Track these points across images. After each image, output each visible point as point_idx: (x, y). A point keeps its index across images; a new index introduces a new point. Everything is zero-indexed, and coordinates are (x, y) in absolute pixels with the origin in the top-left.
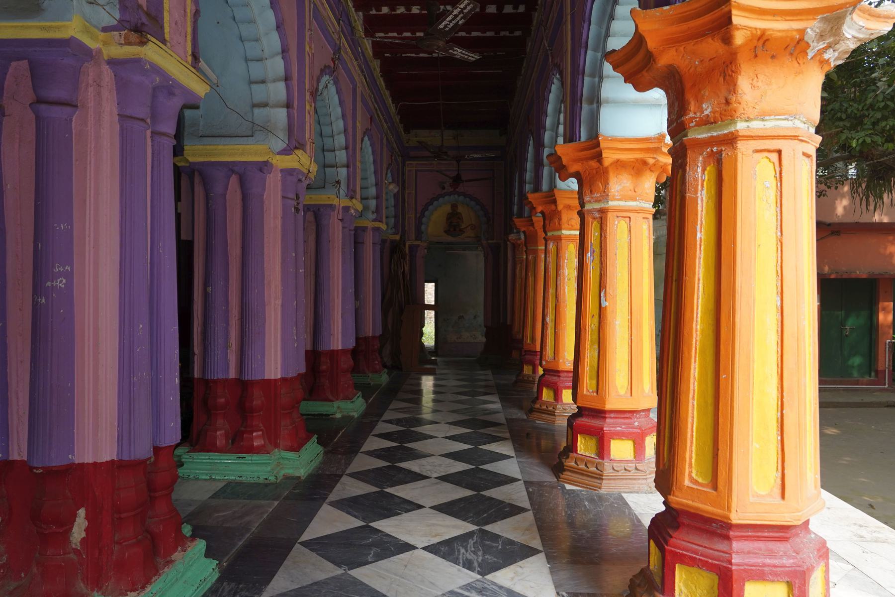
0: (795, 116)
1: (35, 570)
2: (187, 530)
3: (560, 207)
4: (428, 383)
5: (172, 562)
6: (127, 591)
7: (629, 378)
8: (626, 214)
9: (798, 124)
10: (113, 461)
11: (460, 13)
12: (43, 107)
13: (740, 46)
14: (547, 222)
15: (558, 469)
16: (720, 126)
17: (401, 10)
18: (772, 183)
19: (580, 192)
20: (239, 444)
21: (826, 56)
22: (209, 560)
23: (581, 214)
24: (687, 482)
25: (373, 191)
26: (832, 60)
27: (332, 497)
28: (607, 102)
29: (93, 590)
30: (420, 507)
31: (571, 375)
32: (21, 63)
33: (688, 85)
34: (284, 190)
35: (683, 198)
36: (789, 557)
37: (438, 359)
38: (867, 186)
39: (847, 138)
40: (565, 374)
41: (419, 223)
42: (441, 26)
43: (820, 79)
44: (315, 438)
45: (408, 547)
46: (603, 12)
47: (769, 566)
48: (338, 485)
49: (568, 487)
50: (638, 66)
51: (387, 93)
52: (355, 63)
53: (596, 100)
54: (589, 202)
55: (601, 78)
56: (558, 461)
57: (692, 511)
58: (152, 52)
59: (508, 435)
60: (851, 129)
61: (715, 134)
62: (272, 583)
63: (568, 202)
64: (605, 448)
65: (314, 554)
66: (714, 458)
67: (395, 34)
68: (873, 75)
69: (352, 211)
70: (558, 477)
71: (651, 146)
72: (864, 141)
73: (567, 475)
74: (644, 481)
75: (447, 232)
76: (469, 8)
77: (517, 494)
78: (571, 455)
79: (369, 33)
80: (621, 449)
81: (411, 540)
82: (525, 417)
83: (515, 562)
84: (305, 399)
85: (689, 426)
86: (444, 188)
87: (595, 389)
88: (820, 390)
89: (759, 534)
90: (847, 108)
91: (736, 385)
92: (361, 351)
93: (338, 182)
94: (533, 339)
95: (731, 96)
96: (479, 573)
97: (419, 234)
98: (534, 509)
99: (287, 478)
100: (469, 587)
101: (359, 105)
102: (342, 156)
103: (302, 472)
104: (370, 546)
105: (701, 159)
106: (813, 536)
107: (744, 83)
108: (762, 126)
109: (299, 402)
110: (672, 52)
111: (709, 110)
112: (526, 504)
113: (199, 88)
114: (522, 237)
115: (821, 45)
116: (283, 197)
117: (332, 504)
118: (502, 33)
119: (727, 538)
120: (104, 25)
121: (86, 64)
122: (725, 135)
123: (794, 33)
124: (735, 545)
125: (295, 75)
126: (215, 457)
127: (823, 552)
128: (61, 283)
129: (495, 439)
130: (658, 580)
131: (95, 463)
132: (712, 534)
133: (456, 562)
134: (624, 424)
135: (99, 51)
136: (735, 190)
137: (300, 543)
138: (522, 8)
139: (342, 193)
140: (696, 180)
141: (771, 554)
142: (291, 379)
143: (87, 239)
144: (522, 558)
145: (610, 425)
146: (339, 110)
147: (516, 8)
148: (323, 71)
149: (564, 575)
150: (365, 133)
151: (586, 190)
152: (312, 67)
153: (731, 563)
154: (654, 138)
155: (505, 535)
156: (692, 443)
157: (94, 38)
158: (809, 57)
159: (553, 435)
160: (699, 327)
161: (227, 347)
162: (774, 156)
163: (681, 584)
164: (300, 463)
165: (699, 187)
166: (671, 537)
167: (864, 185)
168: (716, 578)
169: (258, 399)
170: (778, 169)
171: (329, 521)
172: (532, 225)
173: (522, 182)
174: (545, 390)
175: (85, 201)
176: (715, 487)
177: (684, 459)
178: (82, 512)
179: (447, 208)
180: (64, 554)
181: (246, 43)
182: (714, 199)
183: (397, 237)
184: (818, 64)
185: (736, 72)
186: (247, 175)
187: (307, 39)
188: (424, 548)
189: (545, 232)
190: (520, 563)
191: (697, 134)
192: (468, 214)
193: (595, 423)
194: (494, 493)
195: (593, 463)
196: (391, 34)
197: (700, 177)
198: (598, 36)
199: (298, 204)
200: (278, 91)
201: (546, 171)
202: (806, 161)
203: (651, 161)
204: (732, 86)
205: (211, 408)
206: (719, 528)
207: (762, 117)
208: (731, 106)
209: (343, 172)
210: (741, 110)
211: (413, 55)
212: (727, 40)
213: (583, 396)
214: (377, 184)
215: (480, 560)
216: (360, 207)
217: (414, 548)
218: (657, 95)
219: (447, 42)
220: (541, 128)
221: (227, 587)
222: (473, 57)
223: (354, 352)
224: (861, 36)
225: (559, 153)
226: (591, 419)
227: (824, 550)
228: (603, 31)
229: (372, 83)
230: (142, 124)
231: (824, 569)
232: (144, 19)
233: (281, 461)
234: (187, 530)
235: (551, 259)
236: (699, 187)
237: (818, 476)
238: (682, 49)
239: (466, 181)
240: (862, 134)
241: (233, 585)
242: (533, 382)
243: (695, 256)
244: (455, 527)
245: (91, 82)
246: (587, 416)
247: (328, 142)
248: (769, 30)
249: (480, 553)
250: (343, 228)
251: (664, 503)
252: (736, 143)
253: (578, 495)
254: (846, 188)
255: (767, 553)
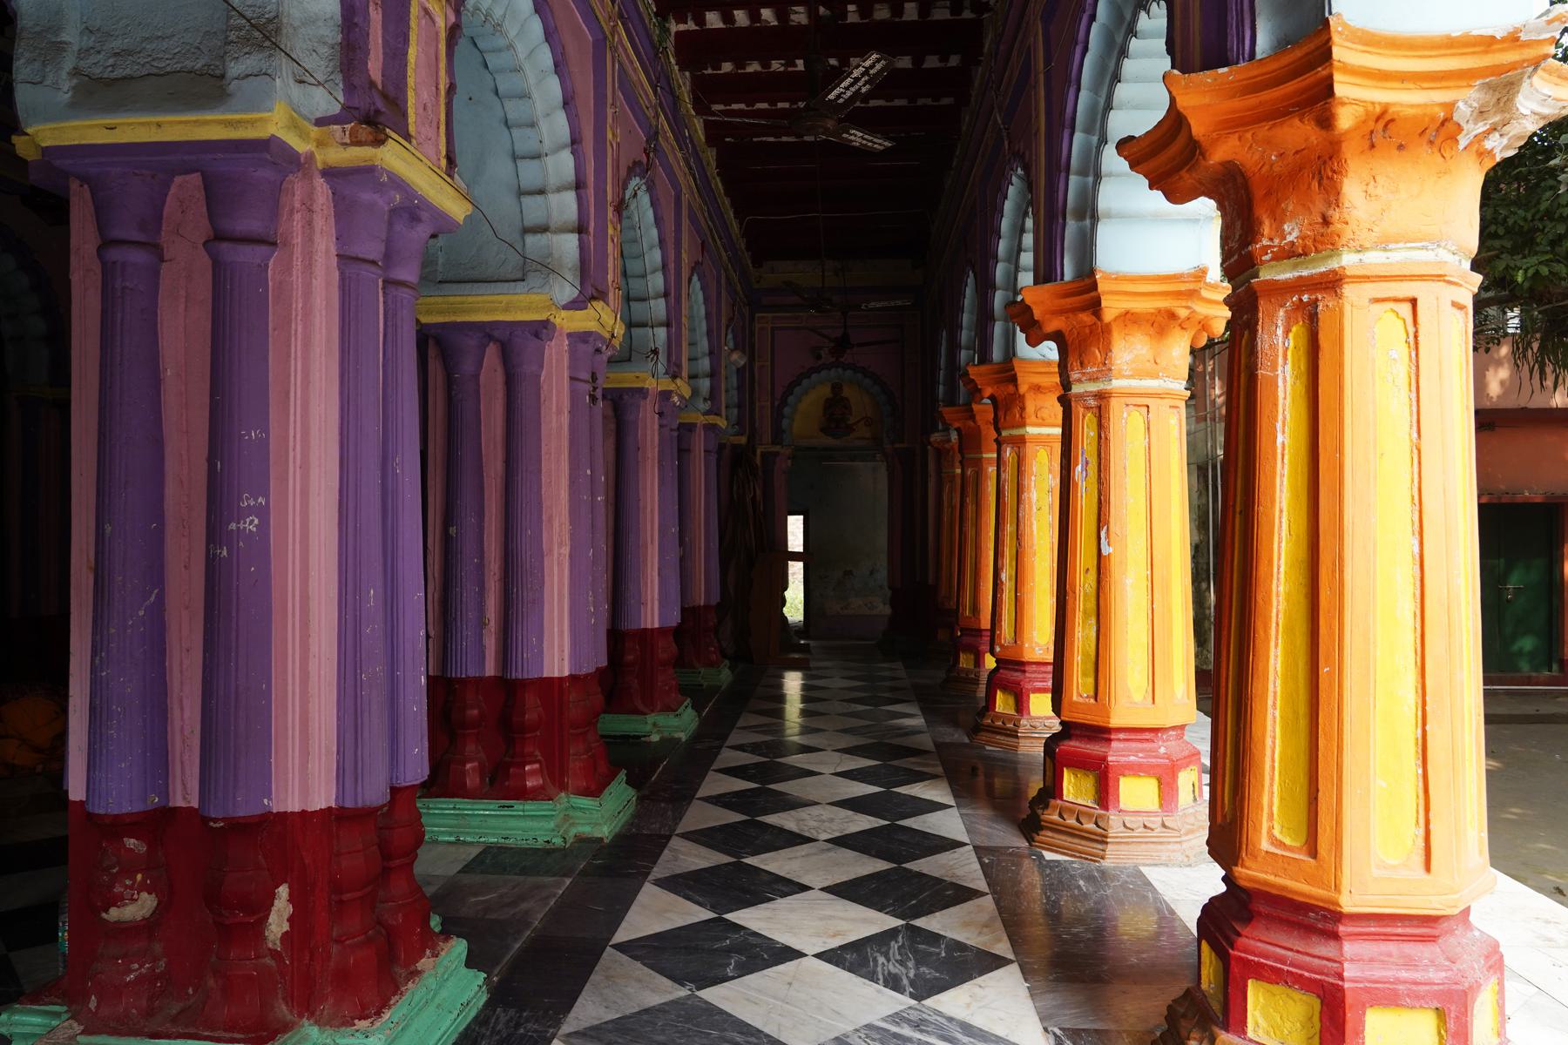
0: (1437, 243)
1: (211, 982)
2: (435, 922)
3: (1023, 389)
4: (793, 683)
5: (418, 973)
6: (353, 1019)
7: (1150, 669)
8: (1143, 401)
9: (1444, 255)
10: (330, 808)
11: (863, 75)
12: (225, 246)
13: (1347, 132)
14: (1001, 414)
15: (1030, 827)
16: (1313, 260)
17: (754, 67)
18: (1402, 352)
19: (1063, 366)
20: (502, 784)
21: (1488, 144)
22: (472, 972)
23: (1065, 401)
24: (1265, 845)
25: (705, 364)
26: (1497, 151)
27: (658, 872)
28: (1109, 216)
29: (301, 1016)
30: (805, 888)
31: (1050, 668)
32: (188, 177)
33: (1258, 193)
34: (572, 367)
35: (1252, 378)
36: (1439, 968)
37: (812, 643)
38: (1542, 348)
39: (1507, 267)
40: (1034, 668)
41: (778, 416)
42: (831, 96)
43: (1479, 180)
44: (622, 775)
45: (790, 954)
46: (1101, 69)
47: (1405, 982)
48: (666, 851)
49: (1049, 856)
50: (1169, 160)
51: (727, 201)
52: (679, 155)
53: (1089, 211)
54: (1079, 381)
55: (1098, 177)
56: (1030, 815)
57: (1274, 891)
58: (392, 156)
59: (939, 770)
60: (1513, 251)
61: (1305, 273)
62: (575, 1009)
63: (1036, 380)
64: (1111, 790)
65: (639, 964)
66: (1310, 804)
67: (742, 106)
68: (1552, 163)
69: (676, 399)
70: (1030, 840)
71: (1183, 287)
72: (1537, 272)
73: (1046, 836)
74: (1177, 847)
75: (824, 430)
76: (878, 67)
77: (964, 867)
78: (1052, 802)
79: (701, 107)
80: (1136, 793)
81: (795, 944)
82: (967, 740)
83: (971, 978)
84: (605, 712)
85: (1268, 752)
86: (819, 357)
87: (1092, 693)
88: (1487, 694)
89: (1389, 930)
90: (1506, 217)
91: (1347, 684)
92: (691, 628)
93: (655, 352)
94: (976, 609)
95: (1331, 212)
96: (912, 996)
97: (778, 435)
98: (994, 892)
99: (581, 840)
100: (897, 1018)
101: (685, 222)
102: (659, 308)
103: (605, 831)
104: (728, 951)
105: (1281, 313)
106: (1477, 933)
107: (1352, 189)
108: (1384, 260)
109: (597, 715)
110: (1233, 141)
111: (1295, 234)
112: (981, 885)
113: (457, 209)
114: (954, 436)
115: (1481, 128)
116: (572, 378)
117: (660, 883)
118: (921, 102)
119: (1336, 937)
120: (319, 115)
121: (291, 177)
122: (1322, 274)
123: (1437, 109)
124: (1349, 948)
125: (591, 179)
126: (466, 806)
127: (1495, 961)
128: (251, 524)
129: (919, 777)
130: (1216, 1006)
131: (304, 812)
132: (1309, 930)
133: (872, 977)
134: (1142, 751)
135: (310, 157)
136: (1341, 365)
137: (613, 946)
138: (954, 61)
139: (661, 368)
140: (1273, 347)
141: (1410, 963)
142: (586, 676)
143: (291, 454)
144: (982, 973)
145: (1117, 753)
146: (654, 232)
147: (944, 59)
148: (631, 172)
149: (1050, 1000)
150: (693, 270)
151: (1073, 362)
152: (617, 167)
153: (1341, 977)
154: (1189, 275)
155: (949, 935)
156: (1272, 779)
157: (304, 136)
158: (1461, 147)
159: (1015, 769)
160: (1281, 588)
161: (482, 624)
162: (1406, 309)
163: (1257, 1013)
164: (599, 816)
165: (1280, 360)
166: (1239, 935)
167: (1536, 346)
168: (1317, 1003)
169: (532, 710)
170: (1411, 330)
171: (655, 912)
172: (973, 417)
173: (954, 346)
174: (999, 695)
175: (288, 393)
176: (1314, 853)
177: (1259, 806)
178: (283, 891)
179: (826, 391)
180: (257, 957)
181: (515, 132)
182: (1304, 378)
183: (743, 440)
184: (1474, 156)
185: (1339, 172)
186: (514, 344)
187: (610, 120)
188: (818, 956)
189: (998, 431)
190: (979, 980)
191: (1273, 273)
192: (859, 401)
193: (1094, 749)
194: (926, 865)
195: (1090, 816)
196: (735, 106)
197: (1280, 345)
198: (1092, 109)
199: (595, 389)
200: (565, 206)
201: (998, 328)
202: (1459, 314)
203: (1183, 313)
204: (1332, 192)
205: (483, 726)
206: (1319, 920)
207: (1384, 244)
208: (1332, 228)
209: (661, 333)
210: (1347, 234)
211: (771, 139)
212: (1326, 121)
213: (1072, 703)
214: (711, 353)
215: (912, 974)
216: (687, 392)
217: (799, 955)
218: (1205, 207)
219: (840, 121)
220: (990, 256)
221: (503, 1016)
222: (880, 144)
223: (678, 633)
224: (1546, 111)
225: (1028, 302)
226: (1084, 742)
227: (1496, 958)
228: (1102, 101)
229: (704, 186)
230: (373, 269)
231: (1496, 988)
232: (380, 104)
233: (571, 813)
234: (435, 922)
235: (1009, 475)
236: (1280, 360)
237: (1485, 835)
238: (1249, 135)
239: (859, 345)
240: (1533, 260)
241: (512, 1012)
242: (976, 682)
243: (1232, 460)
244: (865, 921)
245: (297, 205)
246: (1080, 737)
247: (636, 286)
248: (1394, 104)
249: (911, 964)
250: (661, 426)
251: (1224, 879)
252: (1340, 287)
253: (1066, 870)
254: (1504, 350)
255: (1401, 961)
